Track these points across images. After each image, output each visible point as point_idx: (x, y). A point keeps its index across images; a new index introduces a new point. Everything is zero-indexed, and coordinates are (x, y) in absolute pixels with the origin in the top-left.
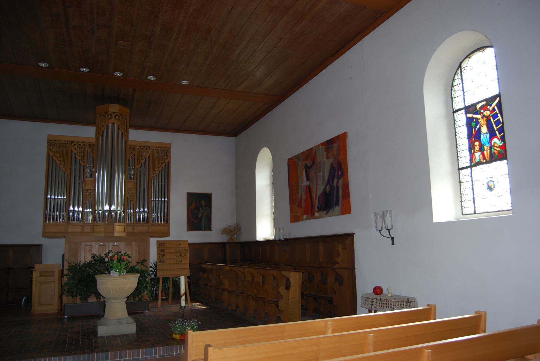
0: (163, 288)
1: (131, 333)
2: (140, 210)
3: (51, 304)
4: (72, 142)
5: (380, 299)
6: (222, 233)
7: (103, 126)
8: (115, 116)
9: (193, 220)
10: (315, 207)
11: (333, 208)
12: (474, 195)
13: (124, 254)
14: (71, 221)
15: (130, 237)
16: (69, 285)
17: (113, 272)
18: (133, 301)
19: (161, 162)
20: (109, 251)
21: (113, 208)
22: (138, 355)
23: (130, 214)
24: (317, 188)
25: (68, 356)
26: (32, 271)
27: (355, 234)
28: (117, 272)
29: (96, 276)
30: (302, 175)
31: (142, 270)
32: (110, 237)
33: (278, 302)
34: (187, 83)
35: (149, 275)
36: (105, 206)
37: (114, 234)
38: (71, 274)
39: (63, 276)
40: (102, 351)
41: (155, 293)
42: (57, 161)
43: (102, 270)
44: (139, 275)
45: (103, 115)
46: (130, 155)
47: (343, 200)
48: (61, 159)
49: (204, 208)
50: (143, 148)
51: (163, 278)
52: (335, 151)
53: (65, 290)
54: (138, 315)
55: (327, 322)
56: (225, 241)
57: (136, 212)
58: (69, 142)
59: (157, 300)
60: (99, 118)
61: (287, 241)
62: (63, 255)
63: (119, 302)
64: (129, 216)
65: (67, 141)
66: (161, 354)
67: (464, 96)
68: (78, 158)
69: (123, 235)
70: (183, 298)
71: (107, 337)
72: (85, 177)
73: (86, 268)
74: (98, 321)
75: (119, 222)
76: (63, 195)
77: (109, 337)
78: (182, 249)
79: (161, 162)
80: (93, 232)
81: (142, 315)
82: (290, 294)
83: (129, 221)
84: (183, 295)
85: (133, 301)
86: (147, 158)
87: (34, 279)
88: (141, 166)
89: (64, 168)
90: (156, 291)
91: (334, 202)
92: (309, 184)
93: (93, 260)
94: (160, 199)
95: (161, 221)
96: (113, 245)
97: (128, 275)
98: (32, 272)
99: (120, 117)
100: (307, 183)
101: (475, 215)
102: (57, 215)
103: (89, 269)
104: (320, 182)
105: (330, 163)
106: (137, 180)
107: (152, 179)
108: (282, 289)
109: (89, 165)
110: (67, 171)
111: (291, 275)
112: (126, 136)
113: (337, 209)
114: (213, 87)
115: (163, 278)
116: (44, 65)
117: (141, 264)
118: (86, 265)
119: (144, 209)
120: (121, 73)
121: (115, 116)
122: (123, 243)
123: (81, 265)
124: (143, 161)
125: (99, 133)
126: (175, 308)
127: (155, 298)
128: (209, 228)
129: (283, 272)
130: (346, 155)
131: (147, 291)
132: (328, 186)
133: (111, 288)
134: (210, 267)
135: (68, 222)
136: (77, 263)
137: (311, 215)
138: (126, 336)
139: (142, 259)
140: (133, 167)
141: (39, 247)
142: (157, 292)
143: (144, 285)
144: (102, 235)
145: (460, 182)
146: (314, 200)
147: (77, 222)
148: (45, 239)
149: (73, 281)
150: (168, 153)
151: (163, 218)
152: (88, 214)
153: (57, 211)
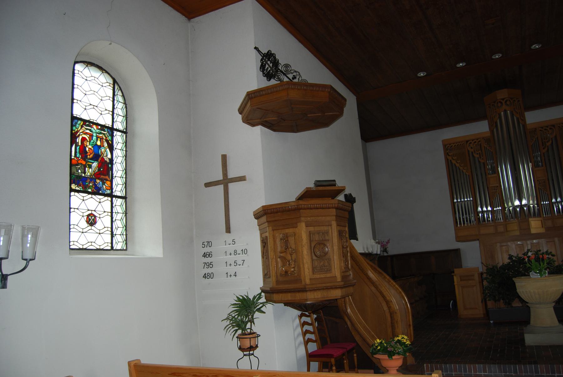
4: (467, 142)
8: (506, 102)
14: (481, 222)
21: (524, 202)
23: (545, 206)
26: (453, 275)
29: (514, 279)
32: (526, 234)
36: (515, 202)
37: (530, 230)
45: (493, 105)
48: (460, 161)
50: (547, 128)
57: (553, 203)
65: (462, 142)
68: (476, 156)
69: (542, 230)
71: (535, 346)
74: (524, 328)
76: (469, 197)
77: (538, 348)
80: (507, 231)
83: (545, 214)
87: (456, 283)
89: (465, 169)
96: (531, 244)
97: (552, 276)
99: (511, 101)
110: (467, 172)
116: (423, 75)
118: (504, 267)
120: (499, 54)
121: (506, 102)
122: (543, 239)
123: (498, 268)
141: (457, 252)
144: (517, 233)
149: (493, 285)
153: (466, 214)
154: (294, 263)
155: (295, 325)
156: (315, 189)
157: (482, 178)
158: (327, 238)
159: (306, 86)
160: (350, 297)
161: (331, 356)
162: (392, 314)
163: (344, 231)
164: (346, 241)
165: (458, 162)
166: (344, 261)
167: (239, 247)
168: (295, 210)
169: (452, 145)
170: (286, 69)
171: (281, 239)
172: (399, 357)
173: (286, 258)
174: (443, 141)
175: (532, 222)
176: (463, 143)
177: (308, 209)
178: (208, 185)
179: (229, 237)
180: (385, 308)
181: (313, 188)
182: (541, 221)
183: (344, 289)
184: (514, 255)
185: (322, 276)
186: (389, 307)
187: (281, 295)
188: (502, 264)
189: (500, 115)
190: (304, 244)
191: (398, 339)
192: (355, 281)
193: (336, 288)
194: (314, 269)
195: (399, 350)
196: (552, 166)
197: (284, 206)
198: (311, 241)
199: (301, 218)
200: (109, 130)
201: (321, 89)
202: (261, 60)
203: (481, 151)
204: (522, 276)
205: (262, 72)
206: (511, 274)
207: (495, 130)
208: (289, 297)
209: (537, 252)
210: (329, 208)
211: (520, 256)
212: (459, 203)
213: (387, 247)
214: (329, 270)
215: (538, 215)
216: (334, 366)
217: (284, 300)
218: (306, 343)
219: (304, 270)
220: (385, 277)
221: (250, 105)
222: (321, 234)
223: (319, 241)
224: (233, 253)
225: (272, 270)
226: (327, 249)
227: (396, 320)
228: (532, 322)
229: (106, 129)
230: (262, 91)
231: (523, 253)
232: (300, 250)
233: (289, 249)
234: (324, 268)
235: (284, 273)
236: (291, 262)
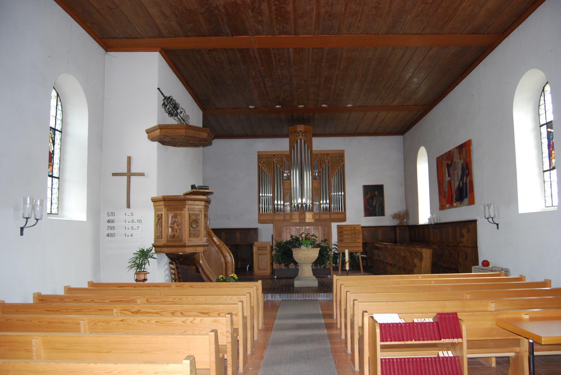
3: (265, 269)
4: (274, 155)
5: (481, 269)
9: (368, 207)
12: (551, 192)
15: (318, 222)
17: (302, 247)
19: (338, 165)
20: (302, 233)
28: (305, 246)
32: (303, 222)
37: (305, 220)
38: (278, 249)
44: (319, 249)
49: (377, 197)
53: (274, 260)
62: (272, 235)
67: (546, 114)
68: (279, 166)
69: (312, 221)
75: (309, 210)
78: (357, 231)
79: (338, 165)
91: (464, 194)
96: (305, 229)
101: (552, 207)
104: (456, 179)
113: (466, 200)
118: (287, 243)
122: (312, 227)
125: (292, 147)
132: (461, 182)
135: (274, 212)
141: (256, 230)
144: (297, 221)
145: (544, 182)
146: (453, 192)
147: (281, 212)
149: (279, 253)
162: (226, 264)
165: (266, 168)
167: (136, 217)
169: (263, 156)
171: (172, 216)
176: (271, 156)
178: (114, 174)
179: (128, 211)
180: (223, 260)
184: (294, 235)
186: (225, 260)
188: (285, 241)
190: (186, 220)
196: (324, 180)
200: (53, 130)
207: (293, 150)
211: (297, 236)
219: (185, 235)
224: (131, 221)
228: (299, 274)
229: (52, 130)
230: (169, 126)
232: (184, 224)
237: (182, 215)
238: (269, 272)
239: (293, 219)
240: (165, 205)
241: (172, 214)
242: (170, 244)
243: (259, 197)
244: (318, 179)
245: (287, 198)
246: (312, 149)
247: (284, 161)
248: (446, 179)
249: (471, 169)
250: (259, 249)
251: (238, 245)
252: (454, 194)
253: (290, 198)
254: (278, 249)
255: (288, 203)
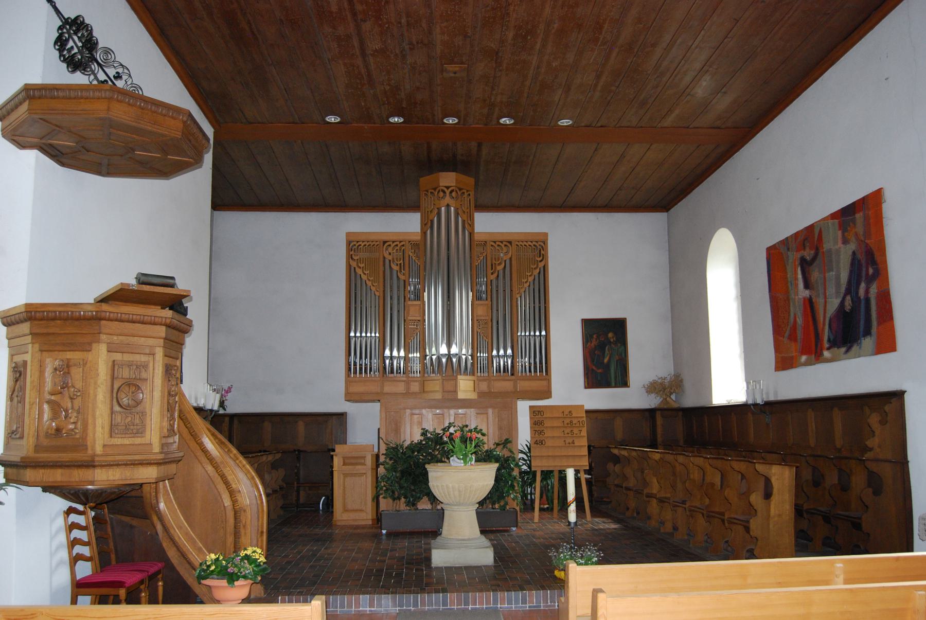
0: (543, 489)
1: (485, 564)
2: (498, 352)
3: (361, 510)
4: (385, 242)
6: (647, 392)
7: (431, 211)
8: (451, 192)
10: (823, 340)
11: (859, 341)
13: (474, 429)
15: (484, 400)
16: (387, 481)
18: (492, 510)
19: (532, 266)
20: (450, 423)
21: (454, 350)
22: (495, 602)
24: (826, 302)
25: (385, 595)
27: (906, 393)
29: (427, 466)
30: (796, 279)
31: (505, 457)
32: (451, 400)
33: (748, 522)
34: (569, 122)
35: (517, 465)
38: (391, 462)
39: (379, 465)
40: (437, 591)
41: (529, 497)
42: (362, 276)
43: (439, 456)
44: (497, 465)
46: (478, 257)
47: (879, 324)
48: (369, 272)
49: (613, 346)
50: (500, 244)
51: (542, 472)
52: (860, 229)
53: (381, 489)
54: (500, 535)
55: (833, 562)
56: (653, 407)
58: (380, 242)
59: (533, 509)
60: (425, 199)
61: (771, 407)
62: (379, 429)
63: (464, 511)
64: (480, 364)
65: (377, 241)
66: (533, 604)
68: (395, 268)
69: (473, 396)
70: (572, 508)
72: (407, 299)
73: (413, 452)
74: (433, 541)
77: (449, 569)
79: (527, 274)
81: (506, 534)
82: (772, 506)
83: (480, 372)
84: (573, 503)
85: (492, 510)
86: (508, 262)
88: (498, 276)
90: (531, 494)
92: (810, 296)
93: (424, 440)
94: (532, 333)
95: (535, 371)
98: (332, 456)
99: (459, 193)
100: (807, 293)
102: (366, 365)
103: (418, 453)
104: (831, 290)
105: (850, 253)
106: (491, 301)
107: (517, 299)
108: (756, 498)
109: (412, 280)
111: (773, 471)
112: (470, 225)
113: (868, 343)
114: (616, 125)
115: (542, 472)
116: (335, 120)
117: (502, 446)
118: (413, 447)
119: (505, 351)
120: (455, 119)
121: (451, 192)
122: (472, 410)
124: (500, 268)
125: (426, 224)
126: (561, 527)
127: (528, 506)
128: (624, 382)
129: (757, 465)
130: (883, 235)
131: (514, 494)
132: (848, 298)
133: (450, 485)
134: (625, 453)
135: (383, 376)
136: (398, 443)
137: (815, 355)
138: (478, 568)
139: (505, 438)
140: (484, 279)
141: (342, 416)
142: (533, 496)
143: (508, 482)
144: (438, 396)
147: (398, 375)
148: (348, 403)
149: (394, 473)
150: (543, 250)
151: (539, 366)
152: (414, 362)
153: (366, 357)
154: (75, 414)
155: (54, 528)
156: (136, 289)
157: (398, 304)
158: (144, 375)
159: (134, 97)
160: (167, 481)
161: (120, 584)
163: (175, 366)
164: (176, 383)
166: (168, 418)
168: (92, 318)
170: (105, 57)
171: (56, 369)
172: (245, 583)
173: (62, 404)
174: (348, 234)
175: (461, 382)
176: (377, 243)
177: (116, 320)
180: (227, 502)
181: (134, 286)
182: (473, 382)
183: (163, 467)
185: (127, 441)
186: (234, 502)
187: (41, 471)
188: (409, 443)
189: (439, 210)
190: (99, 382)
191: (246, 554)
192: (181, 454)
193: (150, 463)
194: (113, 429)
195: (247, 572)
197: (69, 309)
198: (113, 378)
199: (101, 335)
201: (171, 114)
202: (60, 28)
203: (403, 260)
204: (437, 462)
205: (57, 52)
206: (421, 459)
207: (429, 231)
208: (57, 476)
209: (463, 427)
210: (155, 324)
211: (437, 431)
212: (358, 338)
213: (226, 400)
214: (140, 432)
215: (470, 373)
216: (123, 601)
217: (47, 480)
218: (75, 560)
219: (95, 427)
220: (229, 450)
221: (29, 109)
222: (135, 367)
223: (128, 381)
225: (30, 424)
226: (141, 395)
227: (244, 522)
228: (445, 530)
231: (443, 428)
232: (92, 392)
233: (68, 389)
234: (132, 427)
235: (53, 432)
236: (70, 411)
237: (88, 365)
238: (370, 517)
239: (427, 392)
240: (33, 334)
241: (57, 363)
242: (44, 456)
243: (349, 339)
244: (487, 300)
245: (416, 341)
246: (473, 229)
247: (409, 256)
248: (797, 293)
249: (885, 262)
250: (347, 461)
251: (299, 451)
252: (823, 330)
253: (422, 342)
254: (391, 462)
255: (412, 355)
